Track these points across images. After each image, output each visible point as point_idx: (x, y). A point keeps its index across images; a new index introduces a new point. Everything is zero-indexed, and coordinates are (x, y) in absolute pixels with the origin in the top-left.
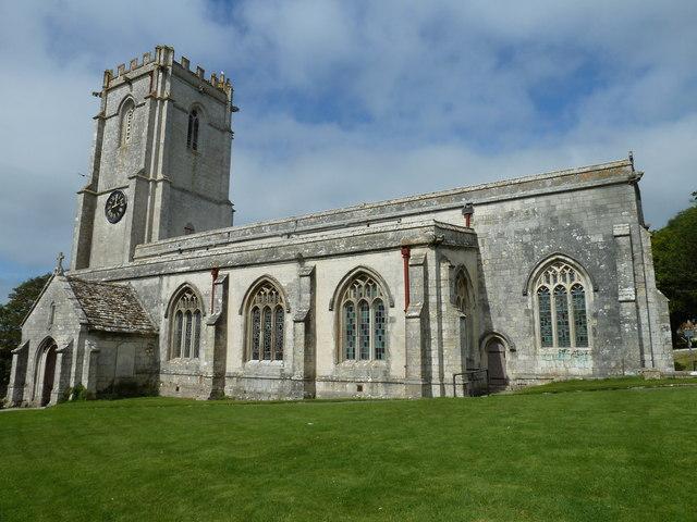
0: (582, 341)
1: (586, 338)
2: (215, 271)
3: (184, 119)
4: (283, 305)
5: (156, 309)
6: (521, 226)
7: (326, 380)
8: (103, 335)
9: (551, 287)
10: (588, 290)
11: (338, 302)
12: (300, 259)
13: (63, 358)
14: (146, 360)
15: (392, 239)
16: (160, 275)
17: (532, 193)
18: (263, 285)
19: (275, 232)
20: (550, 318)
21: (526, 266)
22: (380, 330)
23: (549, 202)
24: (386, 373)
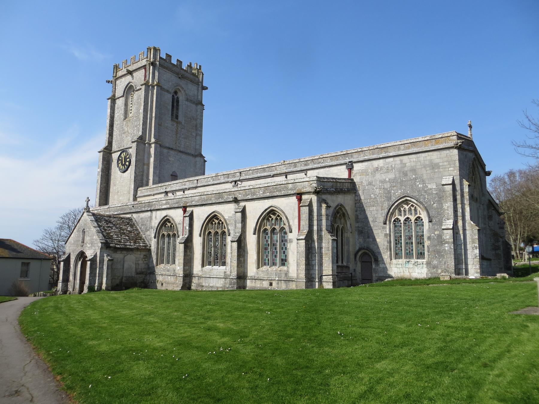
0: (268, 265)
1: (424, 253)
2: (185, 209)
3: (168, 98)
4: (226, 230)
5: (148, 233)
6: (383, 177)
7: (254, 279)
8: (116, 249)
9: (402, 219)
10: (425, 220)
11: (259, 230)
12: (236, 201)
13: (91, 264)
14: (142, 265)
15: (291, 189)
16: (151, 211)
17: (391, 154)
18: (213, 218)
19: (227, 180)
20: (401, 240)
21: (386, 205)
22: (284, 248)
23: (401, 161)
24: (286, 274)
